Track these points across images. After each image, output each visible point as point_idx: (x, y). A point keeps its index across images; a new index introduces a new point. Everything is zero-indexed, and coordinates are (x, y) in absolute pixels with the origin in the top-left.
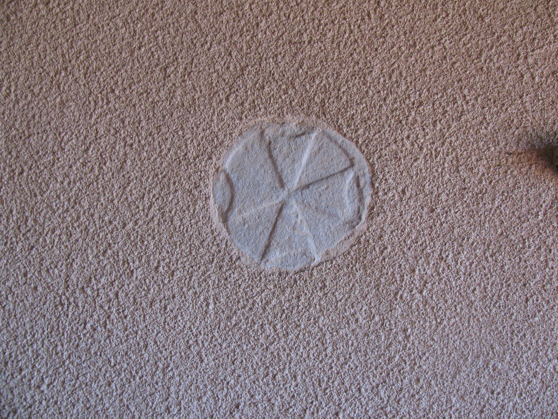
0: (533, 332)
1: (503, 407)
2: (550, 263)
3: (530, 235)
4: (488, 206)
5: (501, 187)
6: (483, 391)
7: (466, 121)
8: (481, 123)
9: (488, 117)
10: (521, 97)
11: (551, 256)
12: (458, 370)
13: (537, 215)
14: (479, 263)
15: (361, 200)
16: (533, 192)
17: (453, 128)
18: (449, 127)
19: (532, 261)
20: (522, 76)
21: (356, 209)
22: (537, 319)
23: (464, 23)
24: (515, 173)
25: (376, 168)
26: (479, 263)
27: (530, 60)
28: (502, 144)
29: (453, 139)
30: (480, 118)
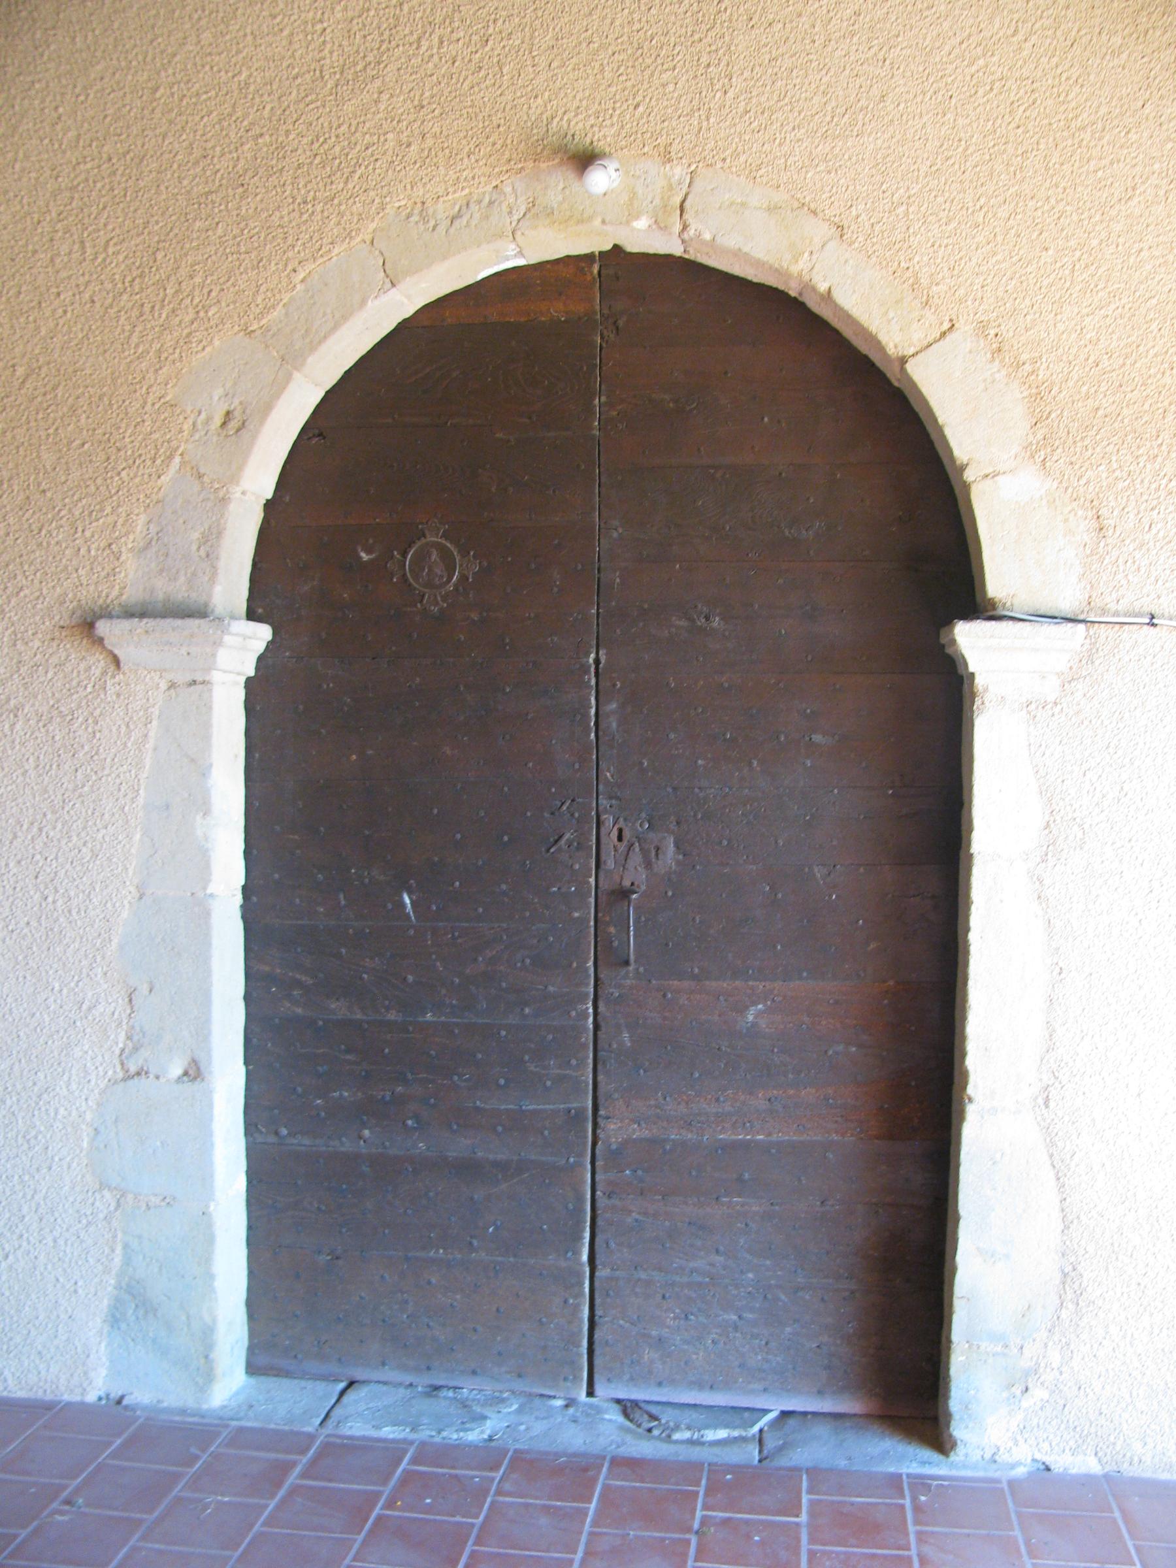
0: (83, 802)
1: (56, 873)
2: (98, 735)
3: (79, 707)
4: (41, 679)
5: (54, 660)
6: (38, 857)
7: (25, 596)
8: (38, 598)
9: (45, 591)
10: (77, 570)
11: (97, 728)
12: (15, 837)
13: (86, 687)
14: (33, 733)
15: (1123, 1511)
16: (82, 666)
17: (13, 603)
18: (9, 602)
19: (80, 732)
20: (79, 550)
21: (660, 856)
22: (86, 789)
23: (28, 498)
24: (68, 646)
25: (103, 1345)
26: (33, 733)
27: (88, 534)
28: (57, 618)
29: (12, 614)
30: (37, 594)
